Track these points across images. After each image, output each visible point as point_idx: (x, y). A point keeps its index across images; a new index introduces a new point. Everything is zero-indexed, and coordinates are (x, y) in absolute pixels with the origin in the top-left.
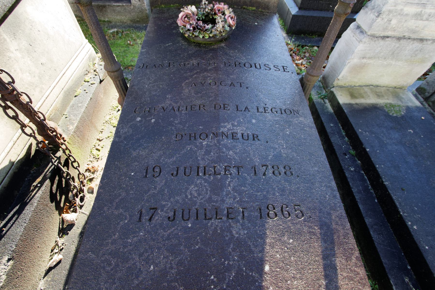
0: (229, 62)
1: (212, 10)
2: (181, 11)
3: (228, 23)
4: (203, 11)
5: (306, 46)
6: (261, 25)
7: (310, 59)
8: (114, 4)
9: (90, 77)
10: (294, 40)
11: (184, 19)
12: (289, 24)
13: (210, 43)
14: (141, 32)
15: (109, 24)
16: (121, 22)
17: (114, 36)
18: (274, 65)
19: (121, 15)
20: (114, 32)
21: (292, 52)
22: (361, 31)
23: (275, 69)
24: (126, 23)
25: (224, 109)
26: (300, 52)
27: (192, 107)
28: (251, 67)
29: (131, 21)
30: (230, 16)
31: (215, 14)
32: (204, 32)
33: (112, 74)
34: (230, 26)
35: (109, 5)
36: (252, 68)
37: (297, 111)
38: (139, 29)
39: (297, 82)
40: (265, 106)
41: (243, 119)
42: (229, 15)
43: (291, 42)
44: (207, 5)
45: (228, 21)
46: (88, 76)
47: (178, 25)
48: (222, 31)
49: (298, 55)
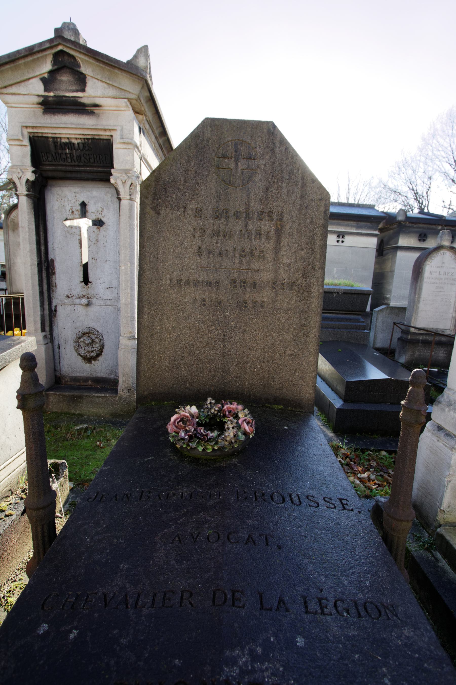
0: (245, 493)
1: (220, 411)
2: (176, 413)
3: (242, 429)
4: (208, 412)
5: (367, 450)
6: (293, 430)
7: (381, 471)
8: (94, 395)
9: (9, 503)
10: (346, 441)
11: (178, 424)
12: (335, 419)
13: (214, 458)
14: (121, 429)
15: (78, 418)
16: (96, 415)
17: (79, 435)
18: (324, 496)
19: (100, 408)
20: (82, 429)
21: (348, 459)
22: (446, 434)
23: (327, 504)
24: (103, 417)
25: (233, 605)
26: (360, 460)
27: (167, 596)
28: (284, 501)
29: (111, 415)
30: (245, 420)
31: (225, 416)
32: (206, 442)
33: (34, 513)
34: (245, 433)
35: (87, 396)
36: (285, 505)
37: (391, 609)
38: (118, 425)
39: (373, 531)
40: (320, 595)
41: (276, 636)
42: (244, 418)
43: (343, 444)
44: (214, 405)
45: (242, 426)
46: (8, 500)
47: (168, 431)
48: (233, 441)
49: (359, 465)
